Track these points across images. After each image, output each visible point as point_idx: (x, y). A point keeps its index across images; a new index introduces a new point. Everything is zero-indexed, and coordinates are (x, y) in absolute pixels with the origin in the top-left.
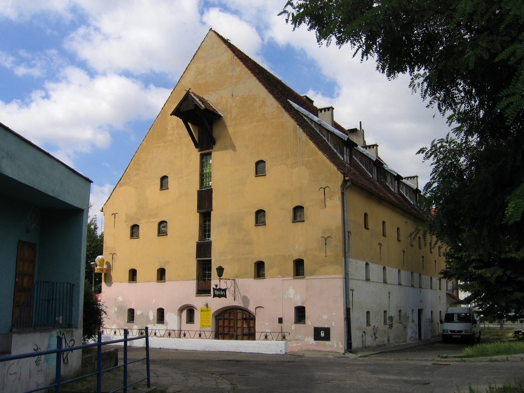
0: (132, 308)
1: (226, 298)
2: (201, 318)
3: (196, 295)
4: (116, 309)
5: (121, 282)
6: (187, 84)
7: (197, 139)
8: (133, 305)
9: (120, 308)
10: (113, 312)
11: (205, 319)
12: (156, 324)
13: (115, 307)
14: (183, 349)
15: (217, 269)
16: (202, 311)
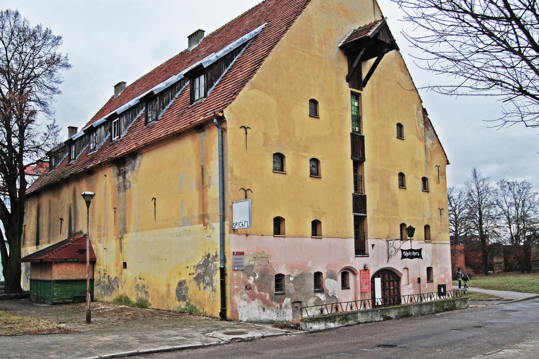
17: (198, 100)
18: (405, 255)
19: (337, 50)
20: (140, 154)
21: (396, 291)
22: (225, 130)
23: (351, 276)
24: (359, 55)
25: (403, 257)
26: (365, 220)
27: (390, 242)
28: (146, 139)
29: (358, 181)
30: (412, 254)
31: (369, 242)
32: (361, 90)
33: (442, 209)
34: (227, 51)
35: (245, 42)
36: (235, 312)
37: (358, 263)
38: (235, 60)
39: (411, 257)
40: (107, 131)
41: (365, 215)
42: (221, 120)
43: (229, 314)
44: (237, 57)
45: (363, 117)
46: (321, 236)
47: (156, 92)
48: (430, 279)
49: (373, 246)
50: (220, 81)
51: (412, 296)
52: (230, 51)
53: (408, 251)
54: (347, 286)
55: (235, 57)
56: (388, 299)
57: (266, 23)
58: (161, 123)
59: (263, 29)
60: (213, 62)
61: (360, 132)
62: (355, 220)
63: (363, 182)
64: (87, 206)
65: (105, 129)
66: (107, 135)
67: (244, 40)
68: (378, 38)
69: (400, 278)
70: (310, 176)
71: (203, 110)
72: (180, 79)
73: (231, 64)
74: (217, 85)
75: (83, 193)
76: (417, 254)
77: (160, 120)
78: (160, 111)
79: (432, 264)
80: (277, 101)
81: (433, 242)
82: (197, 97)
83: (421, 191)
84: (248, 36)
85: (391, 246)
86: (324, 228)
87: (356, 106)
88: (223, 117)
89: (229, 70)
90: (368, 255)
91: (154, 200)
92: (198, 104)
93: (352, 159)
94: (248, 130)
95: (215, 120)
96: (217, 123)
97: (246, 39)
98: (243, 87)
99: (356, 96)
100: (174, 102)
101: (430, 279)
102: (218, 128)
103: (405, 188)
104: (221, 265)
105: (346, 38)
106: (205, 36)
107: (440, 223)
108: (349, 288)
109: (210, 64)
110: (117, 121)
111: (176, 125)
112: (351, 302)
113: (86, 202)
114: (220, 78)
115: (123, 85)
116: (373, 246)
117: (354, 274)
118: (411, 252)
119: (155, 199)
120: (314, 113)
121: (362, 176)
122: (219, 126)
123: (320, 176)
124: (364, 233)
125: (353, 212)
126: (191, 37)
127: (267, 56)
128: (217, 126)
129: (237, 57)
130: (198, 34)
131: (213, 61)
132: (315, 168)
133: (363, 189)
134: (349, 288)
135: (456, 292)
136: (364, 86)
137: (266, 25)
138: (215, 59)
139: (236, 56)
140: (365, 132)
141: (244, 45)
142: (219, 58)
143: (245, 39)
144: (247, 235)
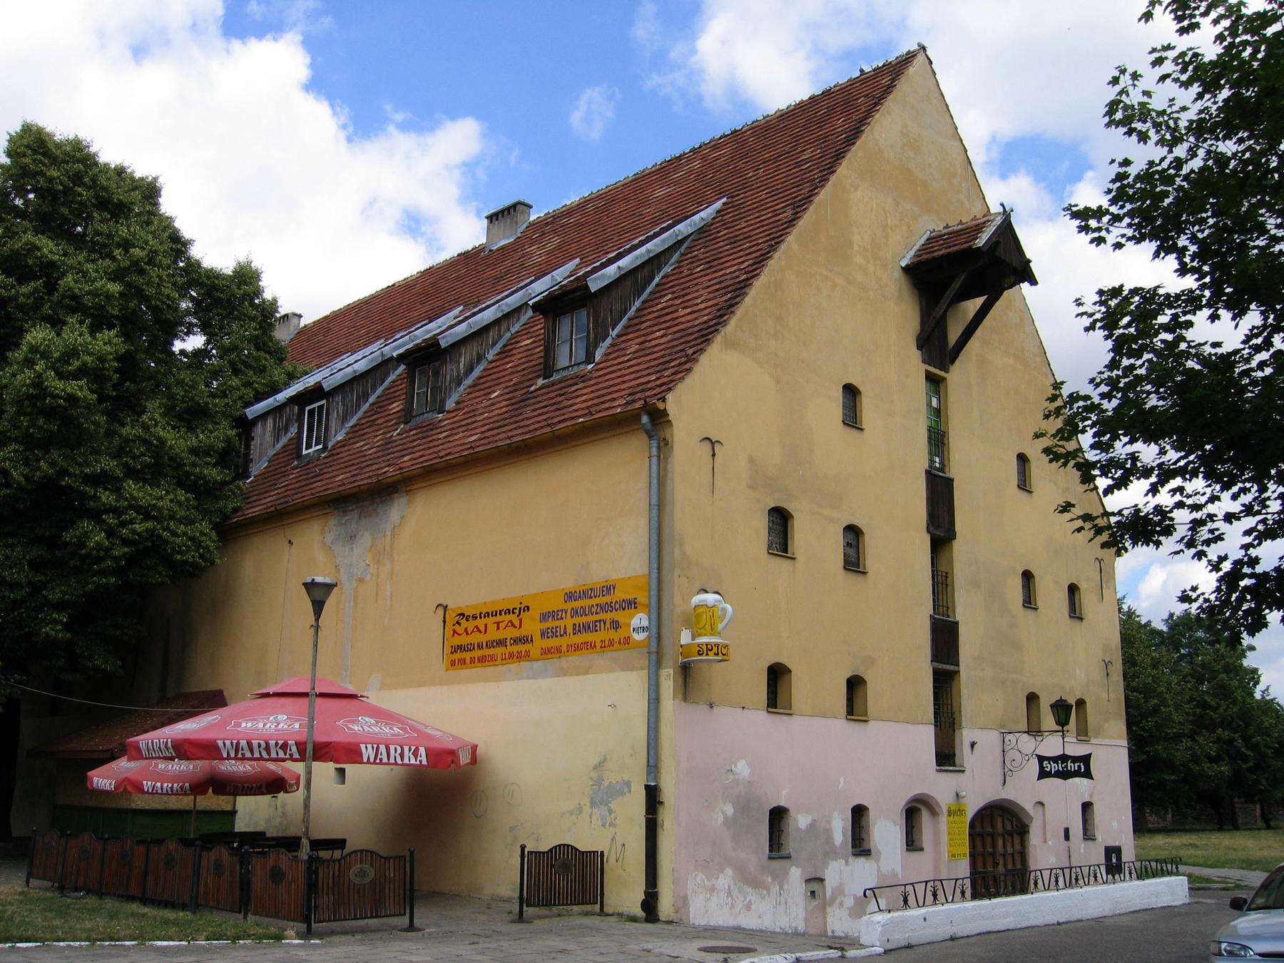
0: (783, 803)
1: (1092, 779)
2: (949, 833)
3: (938, 768)
4: (729, 810)
5: (743, 708)
6: (219, 43)
7: (979, 301)
8: (783, 792)
9: (744, 806)
10: (721, 820)
11: (957, 837)
12: (851, 859)
13: (724, 803)
14: (1079, 917)
15: (1052, 706)
16: (950, 813)
17: (568, 367)
18: (1048, 770)
19: (898, 274)
20: (406, 491)
21: (1017, 858)
22: (667, 444)
23: (925, 816)
24: (950, 290)
25: (1043, 774)
26: (956, 681)
27: (1008, 737)
28: (421, 456)
29: (941, 584)
30: (1067, 766)
31: (967, 734)
32: (947, 371)
33: (1110, 662)
34: (641, 255)
35: (679, 238)
36: (682, 903)
37: (941, 787)
38: (657, 280)
39: (1065, 775)
40: (279, 430)
41: (956, 668)
42: (659, 418)
43: (665, 907)
44: (661, 274)
45: (952, 434)
46: (866, 715)
47: (444, 340)
48: (1088, 835)
49: (973, 745)
50: (626, 327)
51: (938, 884)
52: (647, 258)
53: (1055, 759)
54: (915, 844)
55: (658, 274)
56: (1002, 878)
57: (724, 200)
58: (457, 418)
59: (718, 212)
60: (607, 283)
61: (942, 469)
62: (935, 681)
63: (949, 589)
64: (315, 614)
65: (274, 425)
66: (278, 442)
67: (677, 235)
68: (997, 254)
69: (1028, 826)
70: (844, 567)
71: (592, 392)
72: (500, 315)
73: (649, 289)
74: (619, 336)
75: (309, 580)
76: (1079, 767)
77: (449, 412)
78: (451, 389)
79: (1091, 796)
80: (778, 381)
81: (1093, 741)
82: (563, 361)
83: (1068, 617)
84: (686, 226)
85: (1010, 747)
86: (874, 694)
87: (934, 408)
88: (664, 413)
89: (644, 302)
90: (963, 766)
91: (441, 611)
92: (572, 379)
93: (928, 531)
94: (717, 445)
95: (645, 419)
96: (649, 426)
97: (683, 234)
98: (709, 344)
99: (935, 383)
100: (485, 370)
101: (1088, 835)
102: (650, 437)
103: (1036, 609)
104: (650, 779)
105: (916, 248)
106: (533, 218)
107: (1105, 696)
108: (922, 849)
109: (605, 284)
110: (321, 407)
111: (514, 426)
112: (963, 879)
113: (313, 602)
114: (624, 321)
115: (295, 320)
116: (973, 745)
117: (934, 812)
118: (1062, 764)
119: (446, 608)
120: (852, 419)
121: (947, 573)
122: (654, 433)
123: (865, 568)
124: (953, 713)
125: (932, 661)
126: (494, 218)
127: (758, 274)
128: (647, 432)
129: (661, 274)
130: (515, 210)
131: (610, 277)
132: (852, 550)
133: (950, 605)
134: (922, 849)
135: (1095, 871)
136: (953, 361)
137: (724, 204)
138: (615, 273)
139: (659, 271)
140: (956, 471)
141: (679, 243)
142: (622, 273)
143: (679, 231)
144: (711, 707)
